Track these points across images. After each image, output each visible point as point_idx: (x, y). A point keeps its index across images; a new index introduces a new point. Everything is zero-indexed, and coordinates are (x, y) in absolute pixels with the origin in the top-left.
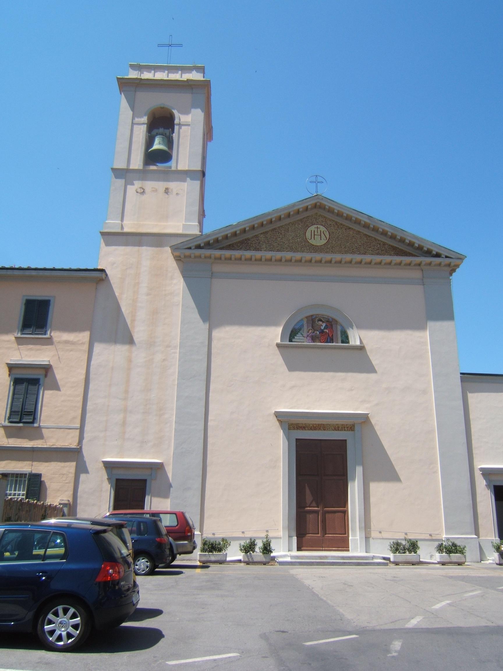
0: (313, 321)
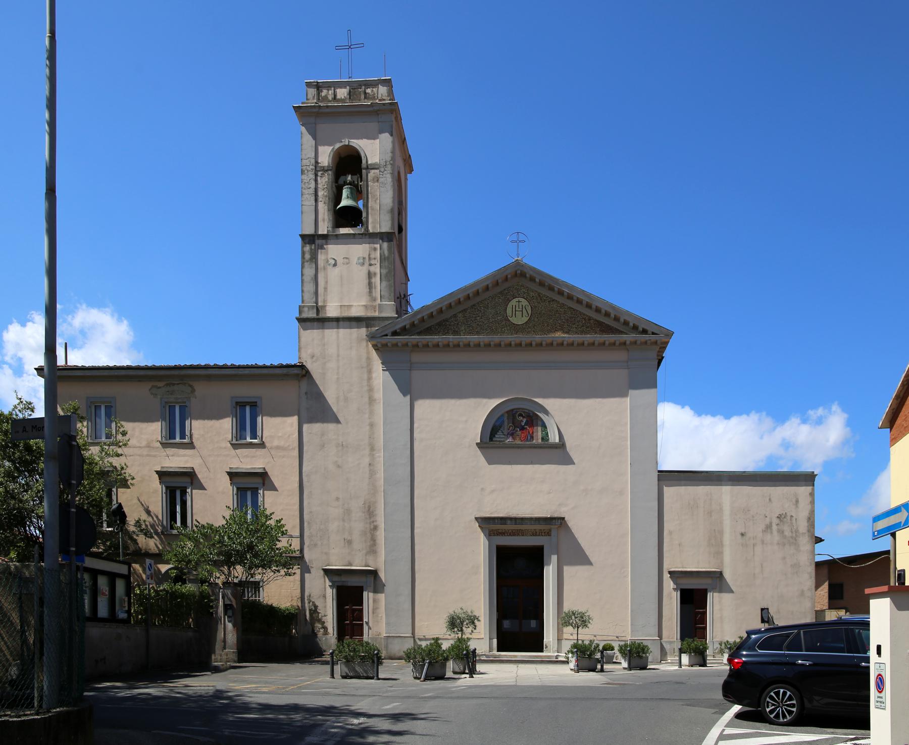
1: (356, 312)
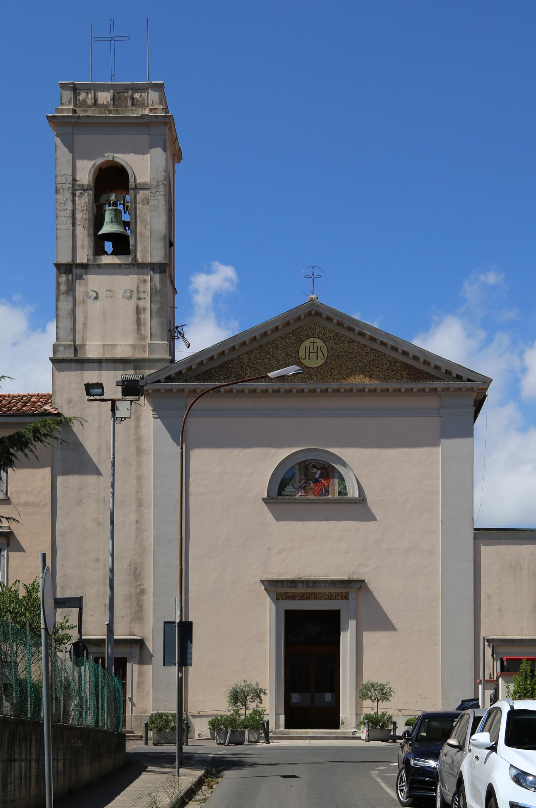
0: (306, 468)
1: (121, 353)
